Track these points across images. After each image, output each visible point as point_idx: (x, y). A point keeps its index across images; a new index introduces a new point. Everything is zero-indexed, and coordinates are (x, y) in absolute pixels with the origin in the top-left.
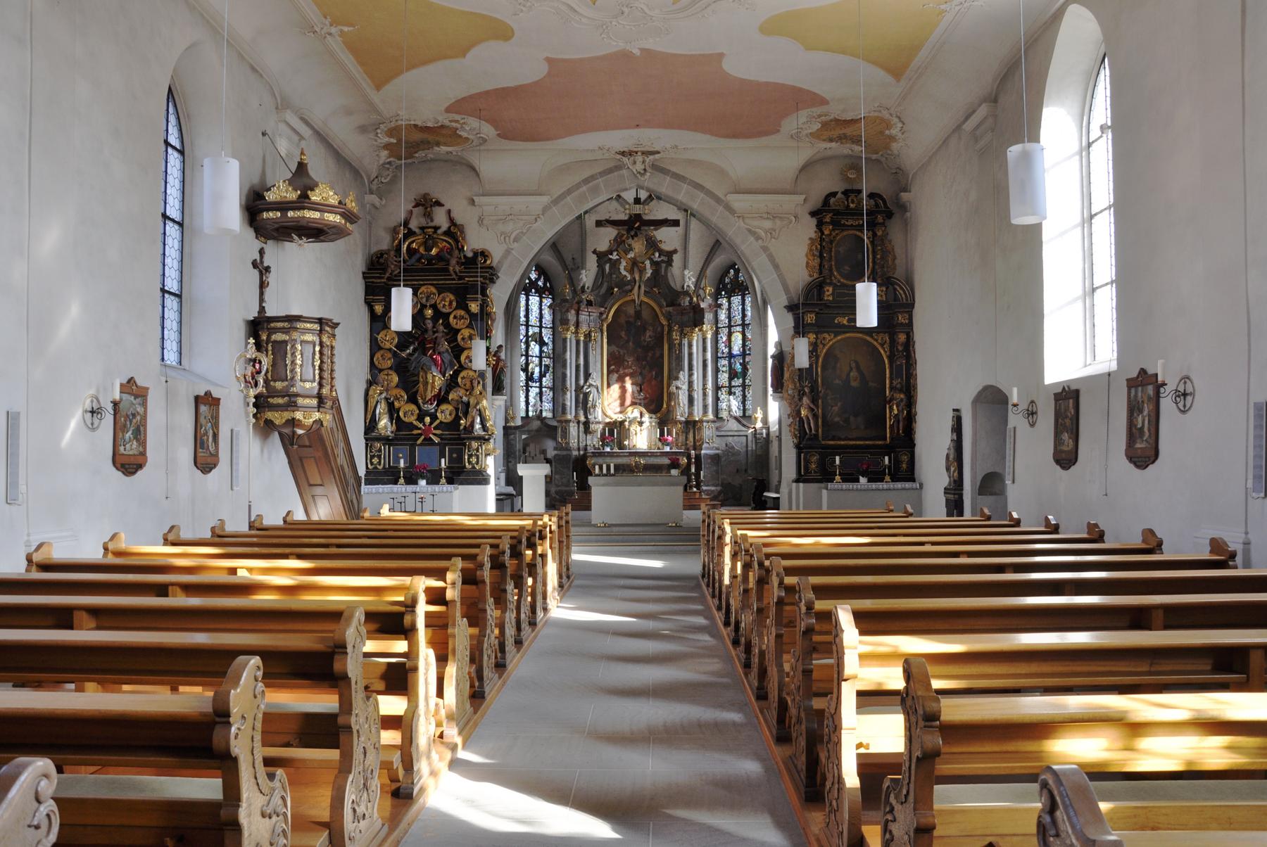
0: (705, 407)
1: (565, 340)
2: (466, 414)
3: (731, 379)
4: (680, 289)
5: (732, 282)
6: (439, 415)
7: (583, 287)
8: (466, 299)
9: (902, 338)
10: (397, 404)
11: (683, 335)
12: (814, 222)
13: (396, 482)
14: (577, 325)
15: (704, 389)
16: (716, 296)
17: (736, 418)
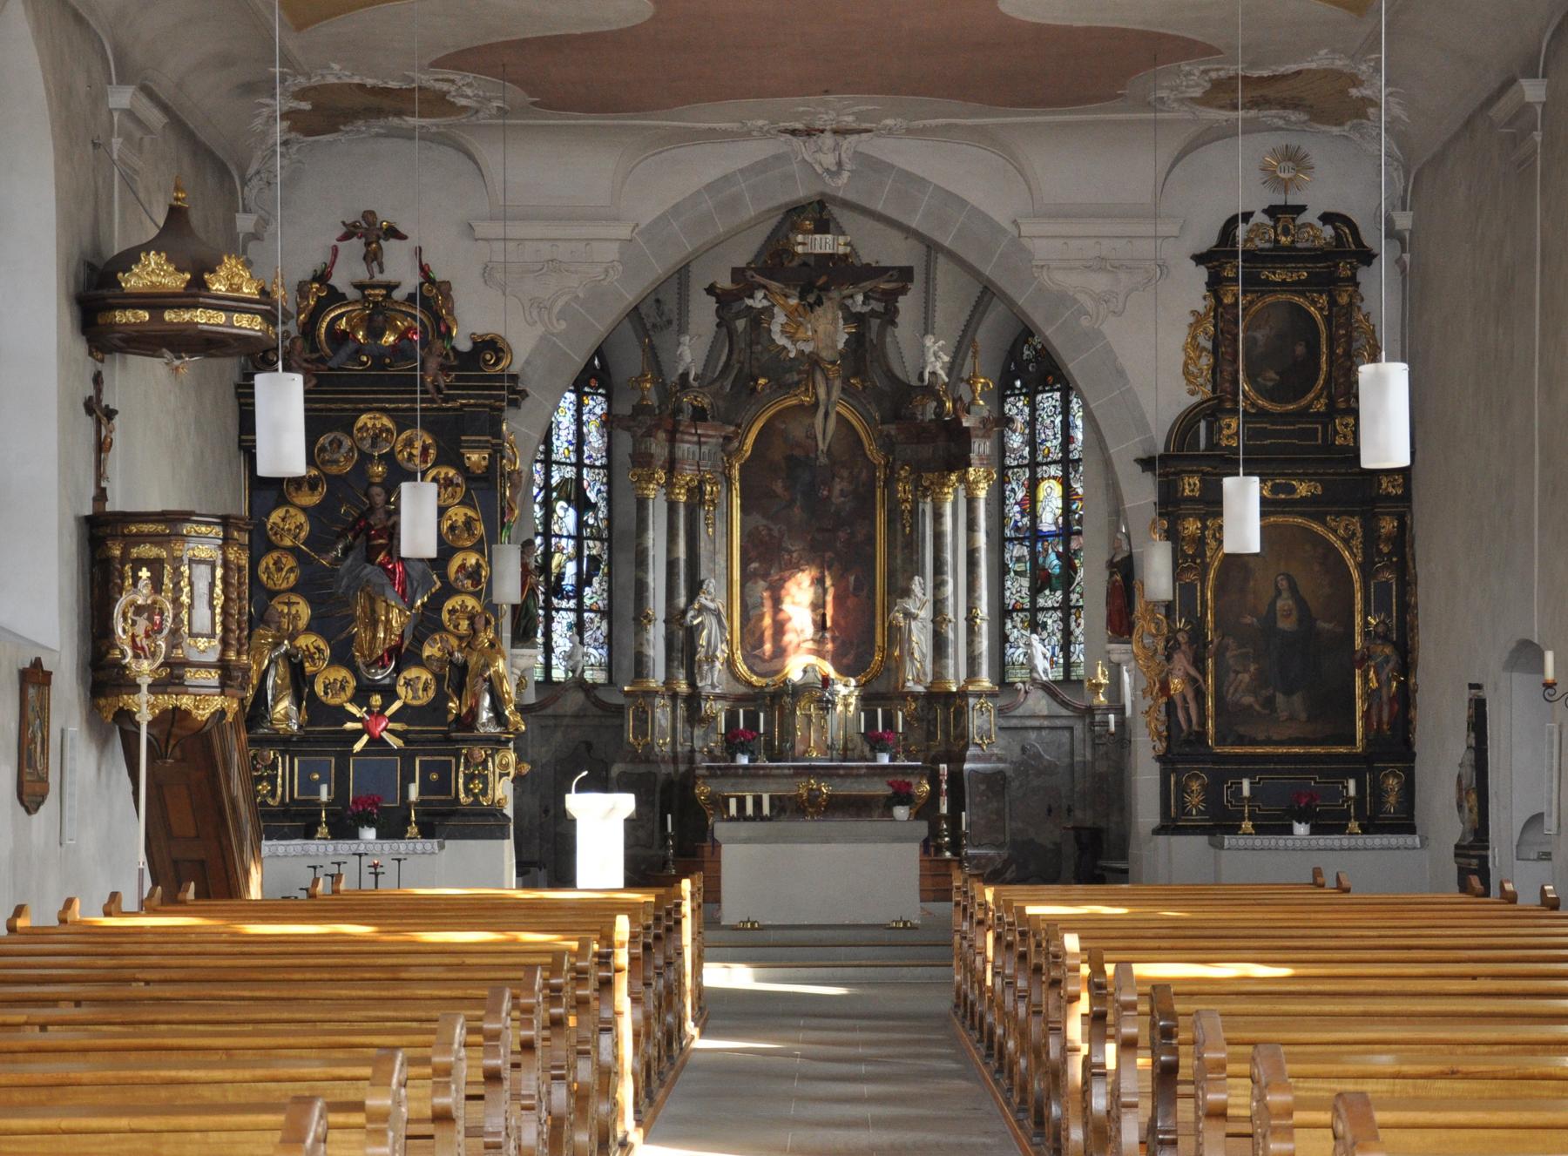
0: (972, 660)
1: (642, 503)
2: (459, 690)
3: (1035, 591)
4: (914, 382)
5: (1033, 366)
6: (401, 690)
7: (685, 375)
8: (459, 444)
9: (1388, 525)
10: (309, 668)
11: (921, 491)
12: (1202, 274)
13: (309, 834)
14: (672, 466)
15: (971, 619)
16: (1003, 391)
17: (1046, 687)
